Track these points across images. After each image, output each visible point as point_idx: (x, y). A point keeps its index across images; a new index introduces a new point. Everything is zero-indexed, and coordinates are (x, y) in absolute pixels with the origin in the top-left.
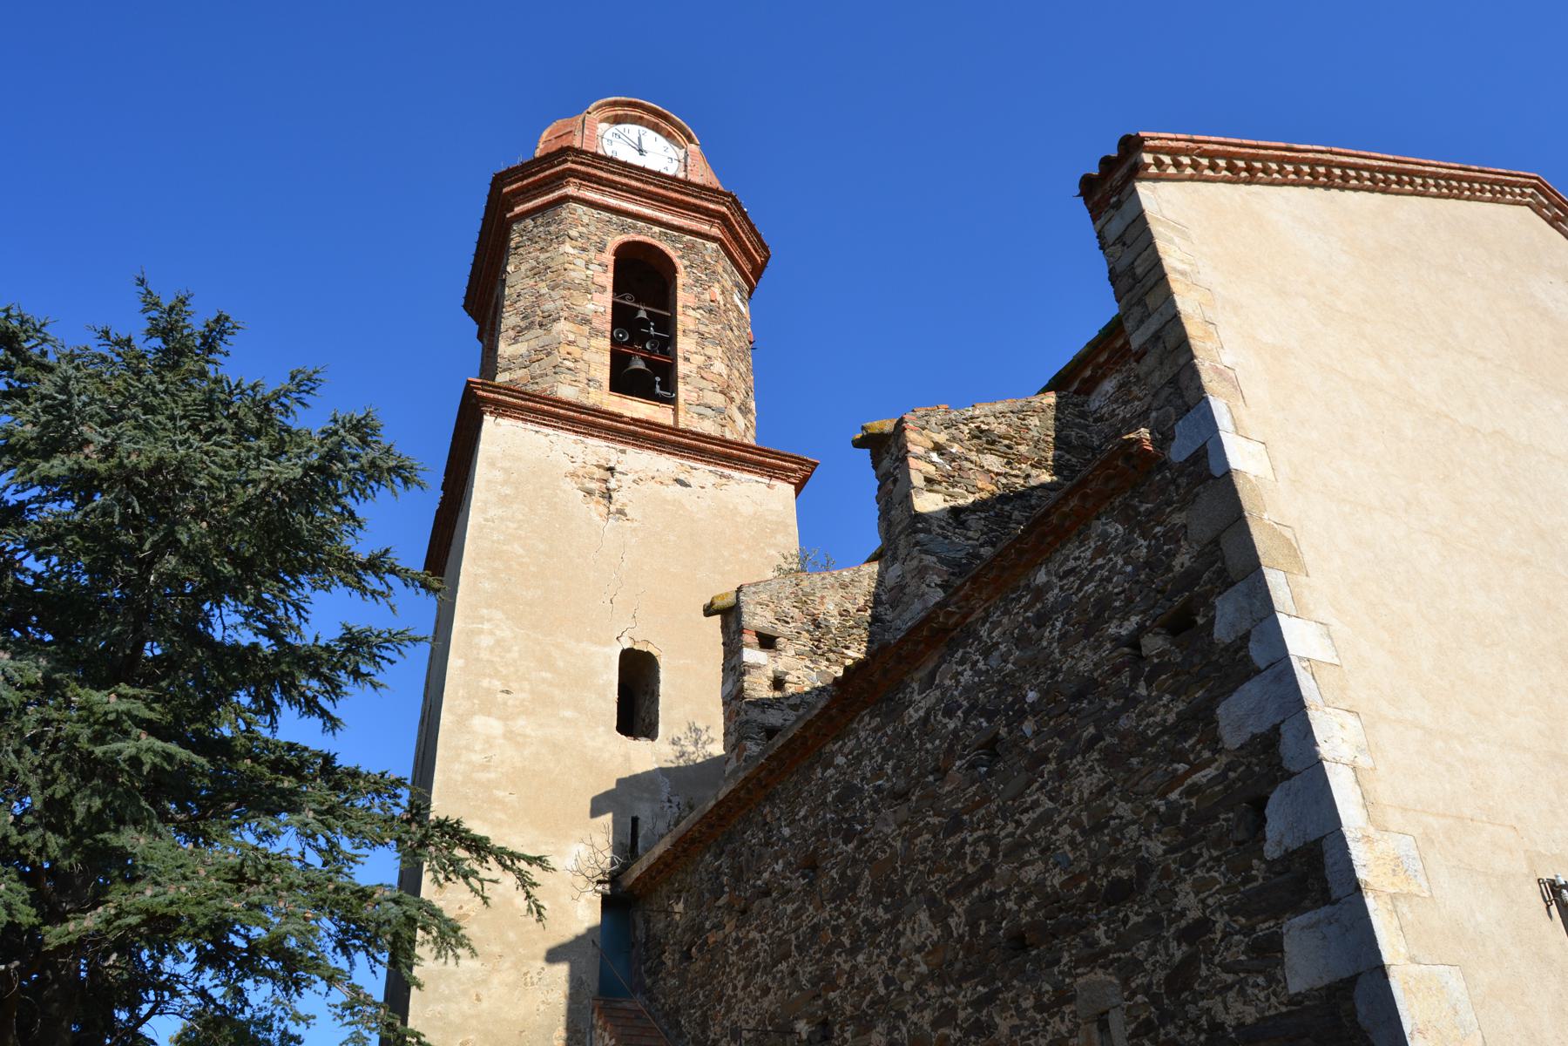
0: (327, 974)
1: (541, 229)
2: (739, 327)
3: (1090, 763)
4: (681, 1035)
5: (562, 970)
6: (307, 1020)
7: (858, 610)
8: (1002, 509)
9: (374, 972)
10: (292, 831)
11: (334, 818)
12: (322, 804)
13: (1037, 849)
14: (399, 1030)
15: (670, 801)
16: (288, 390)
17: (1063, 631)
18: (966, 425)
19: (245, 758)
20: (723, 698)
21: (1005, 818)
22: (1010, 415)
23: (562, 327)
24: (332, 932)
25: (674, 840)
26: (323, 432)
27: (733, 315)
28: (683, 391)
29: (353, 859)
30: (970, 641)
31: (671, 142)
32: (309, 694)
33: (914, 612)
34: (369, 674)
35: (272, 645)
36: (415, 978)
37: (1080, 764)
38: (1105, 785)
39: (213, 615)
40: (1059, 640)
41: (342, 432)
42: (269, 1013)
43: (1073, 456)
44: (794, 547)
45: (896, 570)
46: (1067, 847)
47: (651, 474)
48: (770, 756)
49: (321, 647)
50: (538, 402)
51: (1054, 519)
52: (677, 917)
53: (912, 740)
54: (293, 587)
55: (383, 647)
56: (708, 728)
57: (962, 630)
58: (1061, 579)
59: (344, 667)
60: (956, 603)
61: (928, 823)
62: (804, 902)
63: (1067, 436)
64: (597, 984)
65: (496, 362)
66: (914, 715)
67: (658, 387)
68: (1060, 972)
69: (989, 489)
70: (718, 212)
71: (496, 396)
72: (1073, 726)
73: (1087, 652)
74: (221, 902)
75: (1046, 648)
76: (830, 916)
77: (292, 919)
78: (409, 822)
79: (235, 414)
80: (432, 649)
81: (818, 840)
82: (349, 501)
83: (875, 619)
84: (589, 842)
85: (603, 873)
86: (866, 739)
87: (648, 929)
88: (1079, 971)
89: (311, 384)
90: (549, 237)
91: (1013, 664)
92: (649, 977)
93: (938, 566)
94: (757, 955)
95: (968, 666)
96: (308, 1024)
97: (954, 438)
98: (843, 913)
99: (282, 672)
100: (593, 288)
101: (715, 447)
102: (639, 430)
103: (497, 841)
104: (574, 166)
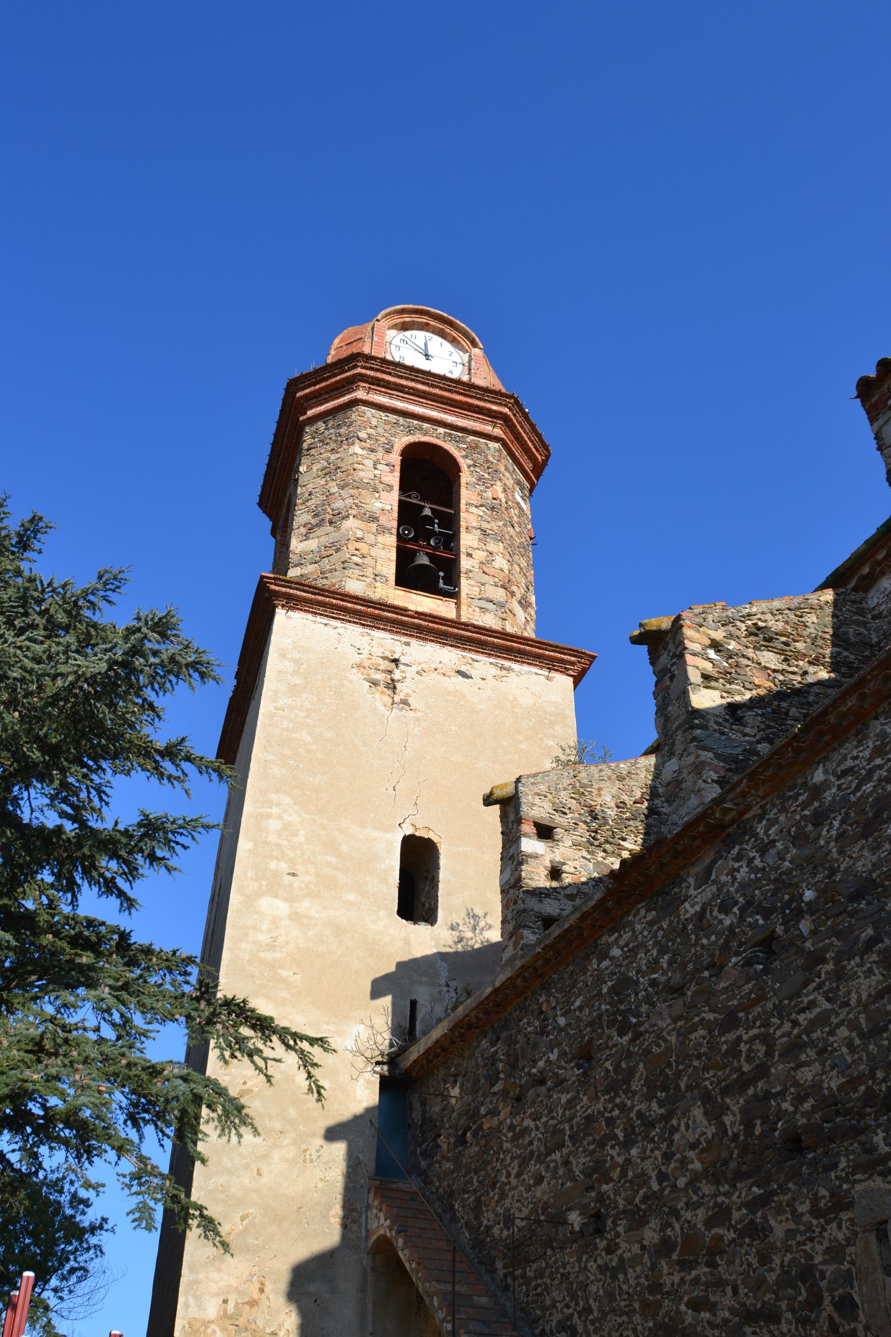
0: (117, 1144)
1: (332, 431)
2: (519, 524)
3: (868, 965)
4: (454, 1219)
5: (340, 1149)
6: (97, 1187)
7: (635, 803)
8: (779, 706)
9: (162, 1145)
10: (89, 1005)
11: (129, 994)
12: (117, 980)
13: (814, 1050)
14: (183, 1202)
15: (447, 985)
16: (96, 589)
17: (841, 830)
18: (743, 622)
19: (47, 933)
20: (501, 887)
21: (781, 1017)
22: (788, 612)
23: (351, 524)
24: (123, 1105)
25: (451, 1024)
26: (127, 629)
27: (514, 512)
28: (466, 586)
29: (145, 1034)
30: (747, 837)
31: (455, 347)
32: (108, 875)
33: (690, 808)
34: (163, 858)
35: (75, 829)
36: (200, 1153)
37: (858, 966)
38: (884, 988)
39: (22, 799)
40: (837, 840)
41: (144, 630)
42: (61, 1175)
43: (851, 653)
44: (572, 739)
45: (673, 765)
46: (845, 1050)
47: (434, 666)
48: (546, 946)
49: (119, 831)
50: (327, 597)
51: (832, 718)
52: (453, 1101)
53: (688, 935)
54: (95, 772)
55: (178, 833)
56: (486, 914)
57: (738, 827)
58: (839, 778)
59: (141, 851)
60: (732, 800)
61: (703, 1019)
62: (578, 1092)
63: (845, 633)
64: (374, 1164)
65: (288, 557)
66: (689, 909)
67: (441, 581)
68: (837, 1178)
69: (767, 685)
70: (501, 413)
71: (288, 590)
72: (851, 926)
73: (866, 853)
74: (22, 1073)
75: (823, 847)
76: (604, 1107)
77: (87, 1092)
78: (198, 999)
79: (47, 610)
80: (222, 835)
81: (593, 1031)
82: (149, 693)
83: (652, 811)
84: (369, 1024)
85: (382, 1054)
86: (641, 933)
87: (424, 1112)
88: (857, 1177)
89: (117, 583)
90: (339, 439)
91: (790, 862)
92: (425, 1159)
93: (715, 762)
94: (531, 1143)
95: (744, 863)
96: (98, 1192)
97: (731, 635)
98: (617, 1106)
99: (84, 855)
100: (381, 487)
101: (496, 640)
102: (423, 623)
103: (281, 1022)
104: (364, 371)
